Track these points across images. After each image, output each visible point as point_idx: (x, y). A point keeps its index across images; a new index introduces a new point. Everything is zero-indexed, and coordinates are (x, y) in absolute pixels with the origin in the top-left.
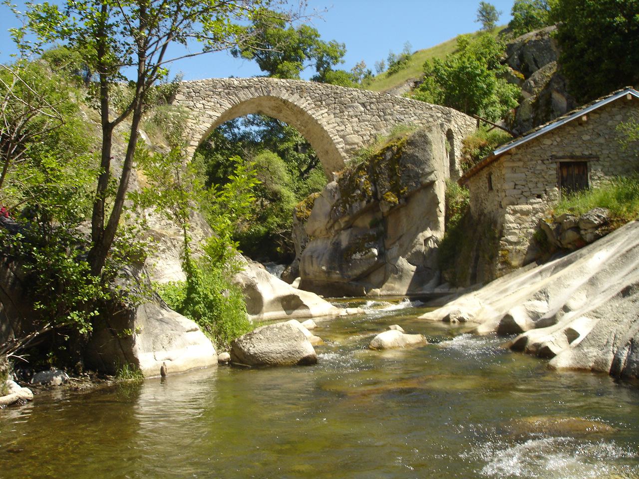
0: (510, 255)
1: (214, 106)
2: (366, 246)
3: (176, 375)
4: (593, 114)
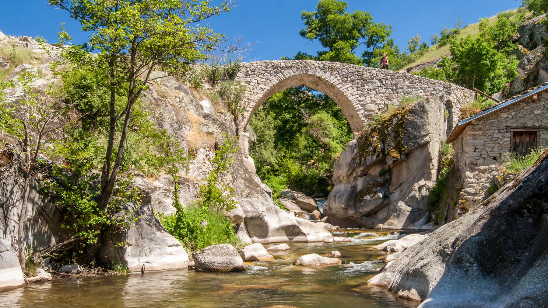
0: (468, 203)
1: (265, 81)
2: (374, 190)
3: (153, 272)
4: (544, 93)
